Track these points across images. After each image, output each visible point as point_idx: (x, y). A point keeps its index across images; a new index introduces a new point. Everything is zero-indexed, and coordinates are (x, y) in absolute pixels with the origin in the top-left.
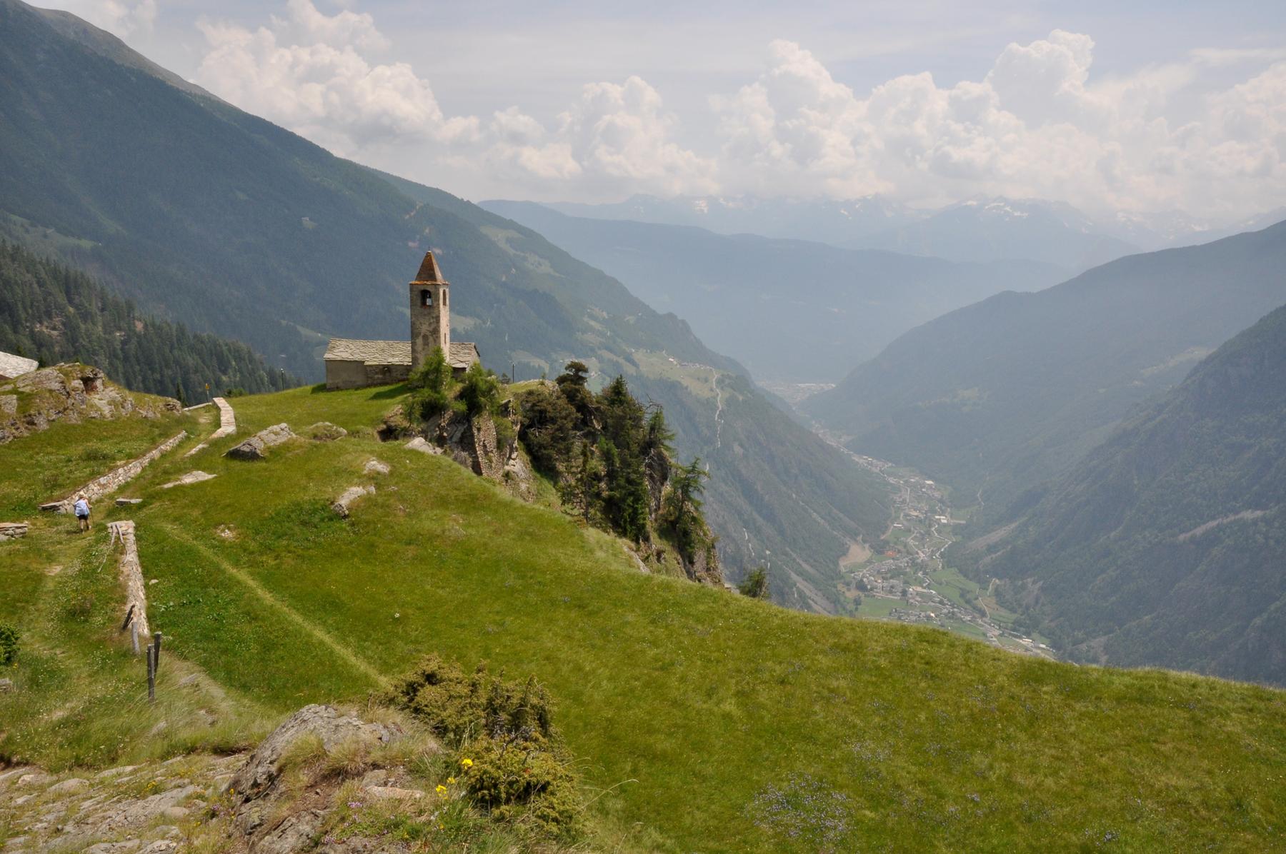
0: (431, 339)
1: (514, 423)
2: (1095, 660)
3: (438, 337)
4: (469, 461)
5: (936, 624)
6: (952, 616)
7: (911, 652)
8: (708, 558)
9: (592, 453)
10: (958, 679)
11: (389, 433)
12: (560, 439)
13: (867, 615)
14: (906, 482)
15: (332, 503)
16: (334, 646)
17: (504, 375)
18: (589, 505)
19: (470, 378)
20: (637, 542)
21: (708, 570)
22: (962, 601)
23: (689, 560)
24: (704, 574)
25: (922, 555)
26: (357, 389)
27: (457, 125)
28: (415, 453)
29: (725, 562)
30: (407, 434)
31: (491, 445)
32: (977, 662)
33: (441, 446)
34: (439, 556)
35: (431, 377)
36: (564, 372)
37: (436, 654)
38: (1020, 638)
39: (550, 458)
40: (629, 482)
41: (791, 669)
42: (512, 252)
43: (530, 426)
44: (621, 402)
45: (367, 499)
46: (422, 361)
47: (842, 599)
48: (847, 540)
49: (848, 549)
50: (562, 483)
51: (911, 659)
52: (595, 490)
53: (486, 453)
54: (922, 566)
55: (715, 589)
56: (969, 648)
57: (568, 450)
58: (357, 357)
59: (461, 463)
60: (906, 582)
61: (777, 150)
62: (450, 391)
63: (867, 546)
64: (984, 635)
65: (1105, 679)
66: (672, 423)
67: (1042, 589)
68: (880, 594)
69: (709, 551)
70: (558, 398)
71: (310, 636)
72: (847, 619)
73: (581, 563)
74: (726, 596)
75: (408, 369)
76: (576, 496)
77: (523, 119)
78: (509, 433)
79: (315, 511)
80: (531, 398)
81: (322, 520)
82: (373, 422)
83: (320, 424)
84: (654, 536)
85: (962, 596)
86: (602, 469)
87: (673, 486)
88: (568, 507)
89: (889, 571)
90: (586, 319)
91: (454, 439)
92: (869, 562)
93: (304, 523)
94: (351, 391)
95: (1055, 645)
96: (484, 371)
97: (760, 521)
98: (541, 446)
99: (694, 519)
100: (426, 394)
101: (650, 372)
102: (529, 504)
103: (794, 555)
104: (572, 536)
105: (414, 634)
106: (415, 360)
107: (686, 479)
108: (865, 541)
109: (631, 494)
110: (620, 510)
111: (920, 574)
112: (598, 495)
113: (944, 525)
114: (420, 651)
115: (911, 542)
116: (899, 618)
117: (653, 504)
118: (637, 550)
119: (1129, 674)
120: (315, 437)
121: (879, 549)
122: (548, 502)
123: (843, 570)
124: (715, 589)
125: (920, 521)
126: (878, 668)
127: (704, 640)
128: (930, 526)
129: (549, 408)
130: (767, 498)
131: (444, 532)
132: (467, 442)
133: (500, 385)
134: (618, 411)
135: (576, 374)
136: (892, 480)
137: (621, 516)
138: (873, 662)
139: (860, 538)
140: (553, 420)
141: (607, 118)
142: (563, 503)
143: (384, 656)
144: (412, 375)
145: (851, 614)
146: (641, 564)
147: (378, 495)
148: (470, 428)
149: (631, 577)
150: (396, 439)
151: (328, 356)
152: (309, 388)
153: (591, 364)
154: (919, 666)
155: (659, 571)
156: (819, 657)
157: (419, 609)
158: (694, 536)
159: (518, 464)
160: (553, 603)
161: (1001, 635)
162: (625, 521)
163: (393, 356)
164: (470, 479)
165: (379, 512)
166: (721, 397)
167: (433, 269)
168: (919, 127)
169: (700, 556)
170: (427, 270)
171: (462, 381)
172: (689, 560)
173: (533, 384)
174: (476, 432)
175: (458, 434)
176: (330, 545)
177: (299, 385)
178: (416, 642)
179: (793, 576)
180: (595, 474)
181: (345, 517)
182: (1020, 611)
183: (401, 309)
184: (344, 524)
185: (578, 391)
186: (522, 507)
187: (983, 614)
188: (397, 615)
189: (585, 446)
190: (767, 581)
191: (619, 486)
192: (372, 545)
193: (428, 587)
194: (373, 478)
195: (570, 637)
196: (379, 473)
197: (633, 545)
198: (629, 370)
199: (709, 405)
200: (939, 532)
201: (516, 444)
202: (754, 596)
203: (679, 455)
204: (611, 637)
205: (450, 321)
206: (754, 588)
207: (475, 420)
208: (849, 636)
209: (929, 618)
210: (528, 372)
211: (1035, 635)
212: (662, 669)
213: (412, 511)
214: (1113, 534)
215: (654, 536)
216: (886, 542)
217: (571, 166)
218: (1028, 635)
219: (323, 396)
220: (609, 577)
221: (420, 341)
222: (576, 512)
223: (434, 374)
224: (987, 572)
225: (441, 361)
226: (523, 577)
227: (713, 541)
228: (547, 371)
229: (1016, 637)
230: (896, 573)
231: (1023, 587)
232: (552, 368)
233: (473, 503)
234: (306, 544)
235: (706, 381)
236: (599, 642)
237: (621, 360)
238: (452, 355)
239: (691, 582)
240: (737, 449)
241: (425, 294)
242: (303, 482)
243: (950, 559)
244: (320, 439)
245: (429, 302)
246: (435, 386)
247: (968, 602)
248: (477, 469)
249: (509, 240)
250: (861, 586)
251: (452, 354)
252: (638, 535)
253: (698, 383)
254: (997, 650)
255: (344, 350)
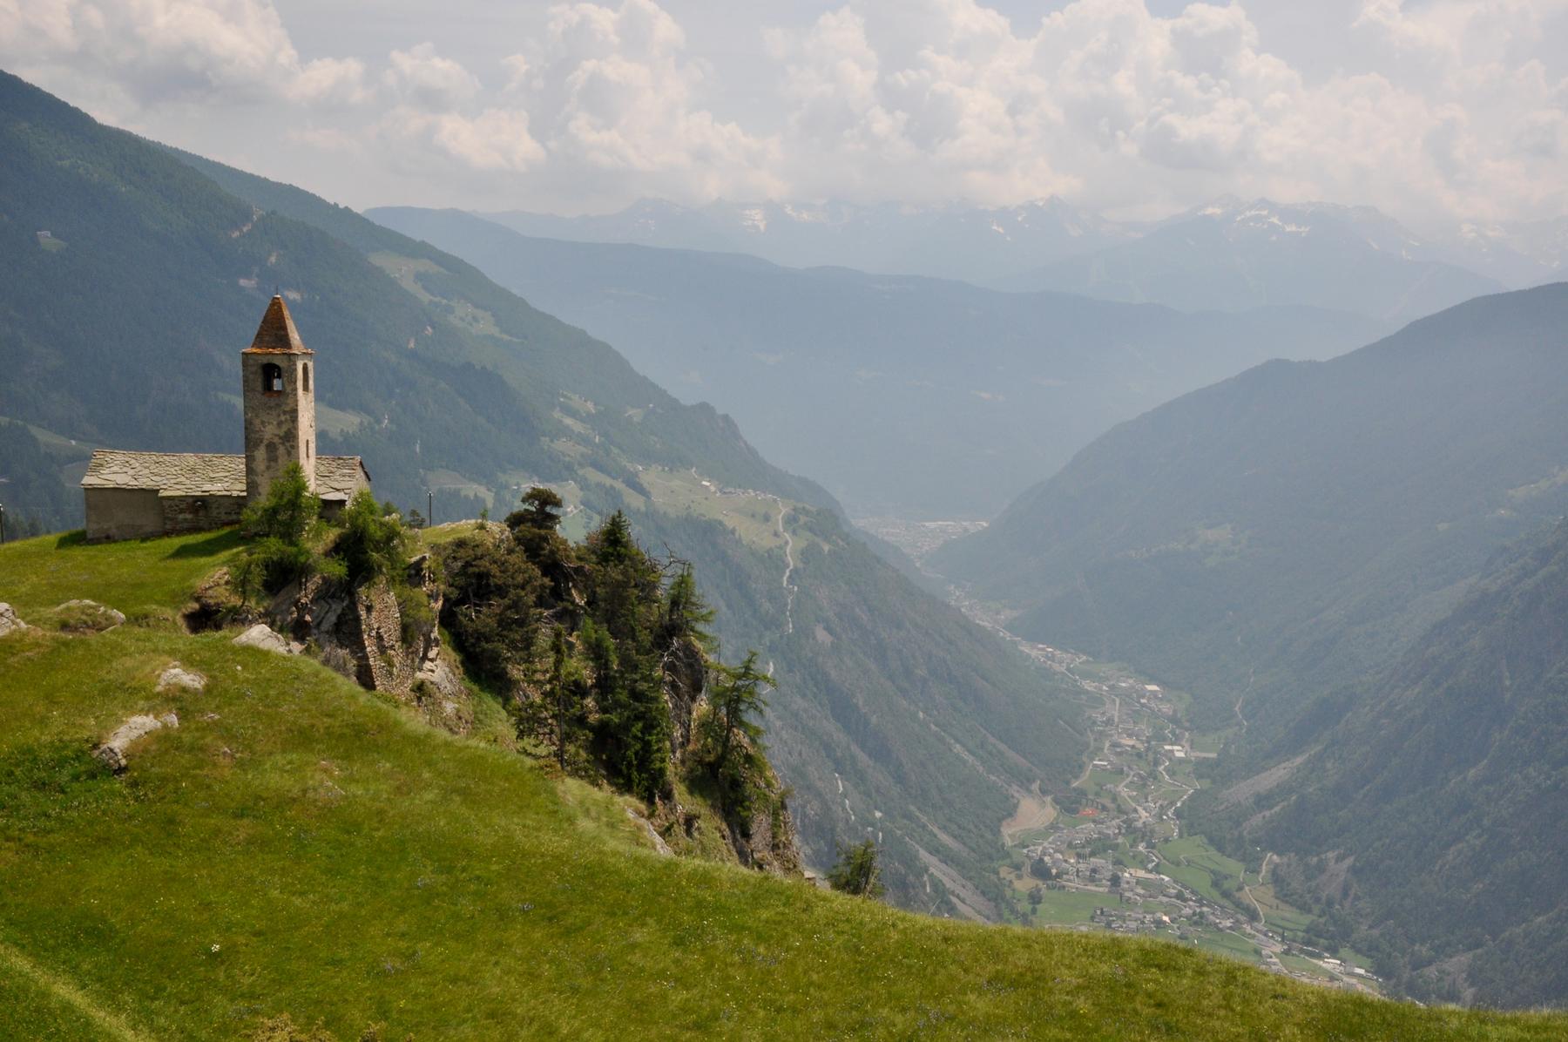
0: (281, 450)
1: (432, 596)
2: (1453, 996)
3: (295, 447)
4: (352, 664)
5: (1171, 935)
6: (1199, 920)
7: (1129, 985)
8: (775, 825)
9: (571, 646)
10: (1214, 1033)
11: (204, 618)
12: (515, 625)
13: (1053, 922)
14: (1112, 687)
15: (96, 746)
16: (93, 1012)
17: (414, 513)
18: (567, 737)
19: (353, 518)
20: (650, 801)
21: (775, 847)
22: (1216, 894)
23: (742, 830)
24: (767, 854)
25: (1144, 814)
26: (143, 540)
27: (324, 74)
28: (251, 651)
29: (803, 834)
30: (238, 618)
31: (391, 634)
32: (1245, 1001)
33: (300, 638)
34: (297, 837)
35: (283, 517)
36: (519, 507)
37: (286, 1016)
38: (1320, 957)
39: (495, 658)
40: (636, 696)
41: (922, 1020)
42: (425, 297)
43: (460, 602)
44: (620, 558)
45: (163, 737)
46: (265, 487)
47: (1008, 893)
48: (1014, 790)
49: (1016, 806)
50: (517, 701)
51: (1131, 998)
52: (576, 711)
53: (383, 650)
54: (1145, 834)
55: (788, 881)
56: (1230, 976)
57: (528, 643)
58: (144, 483)
59: (337, 668)
60: (1118, 862)
61: (882, 123)
62: (317, 542)
63: (1049, 799)
64: (1257, 952)
65: (1473, 1031)
66: (708, 593)
67: (1354, 870)
68: (1074, 884)
69: (775, 814)
70: (510, 551)
71: (45, 995)
72: (1017, 929)
73: (552, 842)
74: (808, 894)
75: (240, 503)
76: (542, 722)
77: (440, 64)
78: (423, 613)
79: (62, 763)
80: (461, 553)
81: (76, 778)
82: (174, 599)
83: (74, 603)
84: (679, 790)
85: (1215, 884)
86: (587, 676)
87: (711, 701)
88: (528, 742)
89: (1088, 842)
90: (557, 414)
91: (325, 626)
92: (1053, 827)
93: (41, 786)
94: (134, 544)
95: (1382, 969)
96: (378, 505)
97: (862, 758)
98: (481, 636)
99: (749, 758)
100: (274, 546)
101: (668, 504)
102: (460, 739)
103: (924, 819)
104: (535, 793)
105: (247, 981)
106: (252, 487)
107: (734, 689)
108: (1044, 792)
109: (639, 717)
110: (620, 745)
111: (1141, 847)
112: (581, 721)
113: (1181, 761)
114: (256, 1013)
115: (1124, 791)
116: (1109, 925)
117: (678, 733)
118: (651, 816)
119: (1514, 1022)
120: (65, 626)
121: (1070, 805)
122: (495, 735)
123: (1009, 842)
124: (788, 881)
125: (1139, 755)
126: (1073, 1015)
127: (770, 973)
128: (1156, 763)
129: (494, 569)
130: (874, 719)
131: (305, 791)
132: (348, 631)
133: (403, 530)
134: (615, 573)
135: (541, 510)
136: (1088, 685)
137: (622, 758)
138: (1065, 1004)
139: (1035, 786)
140: (501, 591)
141: (589, 65)
142: (521, 736)
143: (189, 1025)
144: (247, 514)
145: (1025, 919)
146: (658, 839)
147: (182, 729)
148: (353, 606)
149: (638, 861)
150: (218, 627)
151: (88, 480)
152: (53, 538)
153: (568, 493)
154: (1146, 1011)
155: (689, 852)
156: (972, 997)
157: (258, 934)
158: (749, 788)
159: (440, 669)
160: (503, 915)
161: (1286, 952)
162: (630, 765)
163: (212, 480)
164: (353, 697)
165: (185, 759)
166: (792, 546)
167: (284, 328)
168: (1123, 83)
169: (760, 826)
170: (273, 329)
171: (340, 524)
172: (742, 830)
173: (466, 527)
174: (363, 613)
175: (333, 618)
176: (90, 823)
177: (33, 532)
178: (252, 996)
179: (923, 854)
180: (576, 683)
181: (121, 770)
182: (1316, 909)
183: (226, 397)
184: (118, 784)
185: (545, 539)
186: (447, 744)
187: (1253, 916)
188: (216, 948)
189: (558, 635)
190: (878, 863)
191: (617, 704)
192: (171, 821)
193: (275, 893)
194: (174, 699)
195: (533, 976)
196: (184, 690)
197: (643, 807)
198: (633, 501)
199: (773, 560)
200: (1172, 772)
201: (435, 634)
202: (856, 890)
203: (722, 645)
204: (606, 973)
205: (317, 418)
206: (854, 876)
207: (362, 591)
208: (1022, 958)
209: (1159, 924)
210: (455, 506)
211: (1345, 952)
212: (697, 1026)
213: (247, 755)
214: (1472, 772)
215: (679, 790)
216: (1082, 793)
217: (527, 148)
218: (1334, 953)
219: (79, 553)
220: (601, 864)
221: (261, 454)
222: (542, 750)
223: (288, 510)
224: (1256, 842)
225: (300, 488)
226: (449, 870)
227: (783, 796)
228: (490, 505)
229: (1312, 955)
230: (1100, 846)
231: (1321, 868)
232: (499, 499)
233: (359, 740)
234: (42, 823)
235: (767, 518)
236: (585, 983)
237: (619, 485)
238: (317, 478)
239: (744, 870)
240: (822, 635)
241: (270, 371)
242: (40, 709)
243: (1192, 819)
244: (74, 629)
245: (277, 384)
246: (289, 533)
247: (1226, 895)
248: (366, 679)
249: (419, 277)
250: (1040, 871)
251: (320, 476)
252: (652, 789)
253: (754, 524)
254: (1280, 980)
255: (119, 470)
